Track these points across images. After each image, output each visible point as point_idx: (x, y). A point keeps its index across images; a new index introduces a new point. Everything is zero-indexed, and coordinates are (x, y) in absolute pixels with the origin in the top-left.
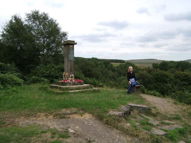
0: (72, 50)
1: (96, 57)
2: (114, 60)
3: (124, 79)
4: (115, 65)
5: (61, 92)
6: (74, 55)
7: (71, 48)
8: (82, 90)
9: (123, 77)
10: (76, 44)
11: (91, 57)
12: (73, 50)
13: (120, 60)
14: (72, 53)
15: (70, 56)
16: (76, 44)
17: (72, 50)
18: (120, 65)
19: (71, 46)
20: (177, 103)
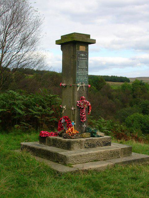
0: (84, 57)
1: (122, 76)
2: (124, 78)
3: (131, 112)
4: (115, 86)
5: (24, 123)
6: (87, 70)
7: (82, 52)
8: (23, 123)
9: (129, 108)
10: (93, 42)
11: (119, 76)
12: (87, 57)
13: (121, 77)
14: (85, 67)
15: (79, 72)
16: (93, 42)
17: (84, 57)
18: (123, 86)
19: (82, 48)
20: (57, 172)
